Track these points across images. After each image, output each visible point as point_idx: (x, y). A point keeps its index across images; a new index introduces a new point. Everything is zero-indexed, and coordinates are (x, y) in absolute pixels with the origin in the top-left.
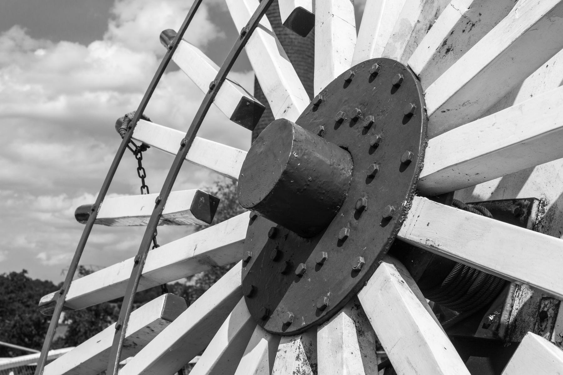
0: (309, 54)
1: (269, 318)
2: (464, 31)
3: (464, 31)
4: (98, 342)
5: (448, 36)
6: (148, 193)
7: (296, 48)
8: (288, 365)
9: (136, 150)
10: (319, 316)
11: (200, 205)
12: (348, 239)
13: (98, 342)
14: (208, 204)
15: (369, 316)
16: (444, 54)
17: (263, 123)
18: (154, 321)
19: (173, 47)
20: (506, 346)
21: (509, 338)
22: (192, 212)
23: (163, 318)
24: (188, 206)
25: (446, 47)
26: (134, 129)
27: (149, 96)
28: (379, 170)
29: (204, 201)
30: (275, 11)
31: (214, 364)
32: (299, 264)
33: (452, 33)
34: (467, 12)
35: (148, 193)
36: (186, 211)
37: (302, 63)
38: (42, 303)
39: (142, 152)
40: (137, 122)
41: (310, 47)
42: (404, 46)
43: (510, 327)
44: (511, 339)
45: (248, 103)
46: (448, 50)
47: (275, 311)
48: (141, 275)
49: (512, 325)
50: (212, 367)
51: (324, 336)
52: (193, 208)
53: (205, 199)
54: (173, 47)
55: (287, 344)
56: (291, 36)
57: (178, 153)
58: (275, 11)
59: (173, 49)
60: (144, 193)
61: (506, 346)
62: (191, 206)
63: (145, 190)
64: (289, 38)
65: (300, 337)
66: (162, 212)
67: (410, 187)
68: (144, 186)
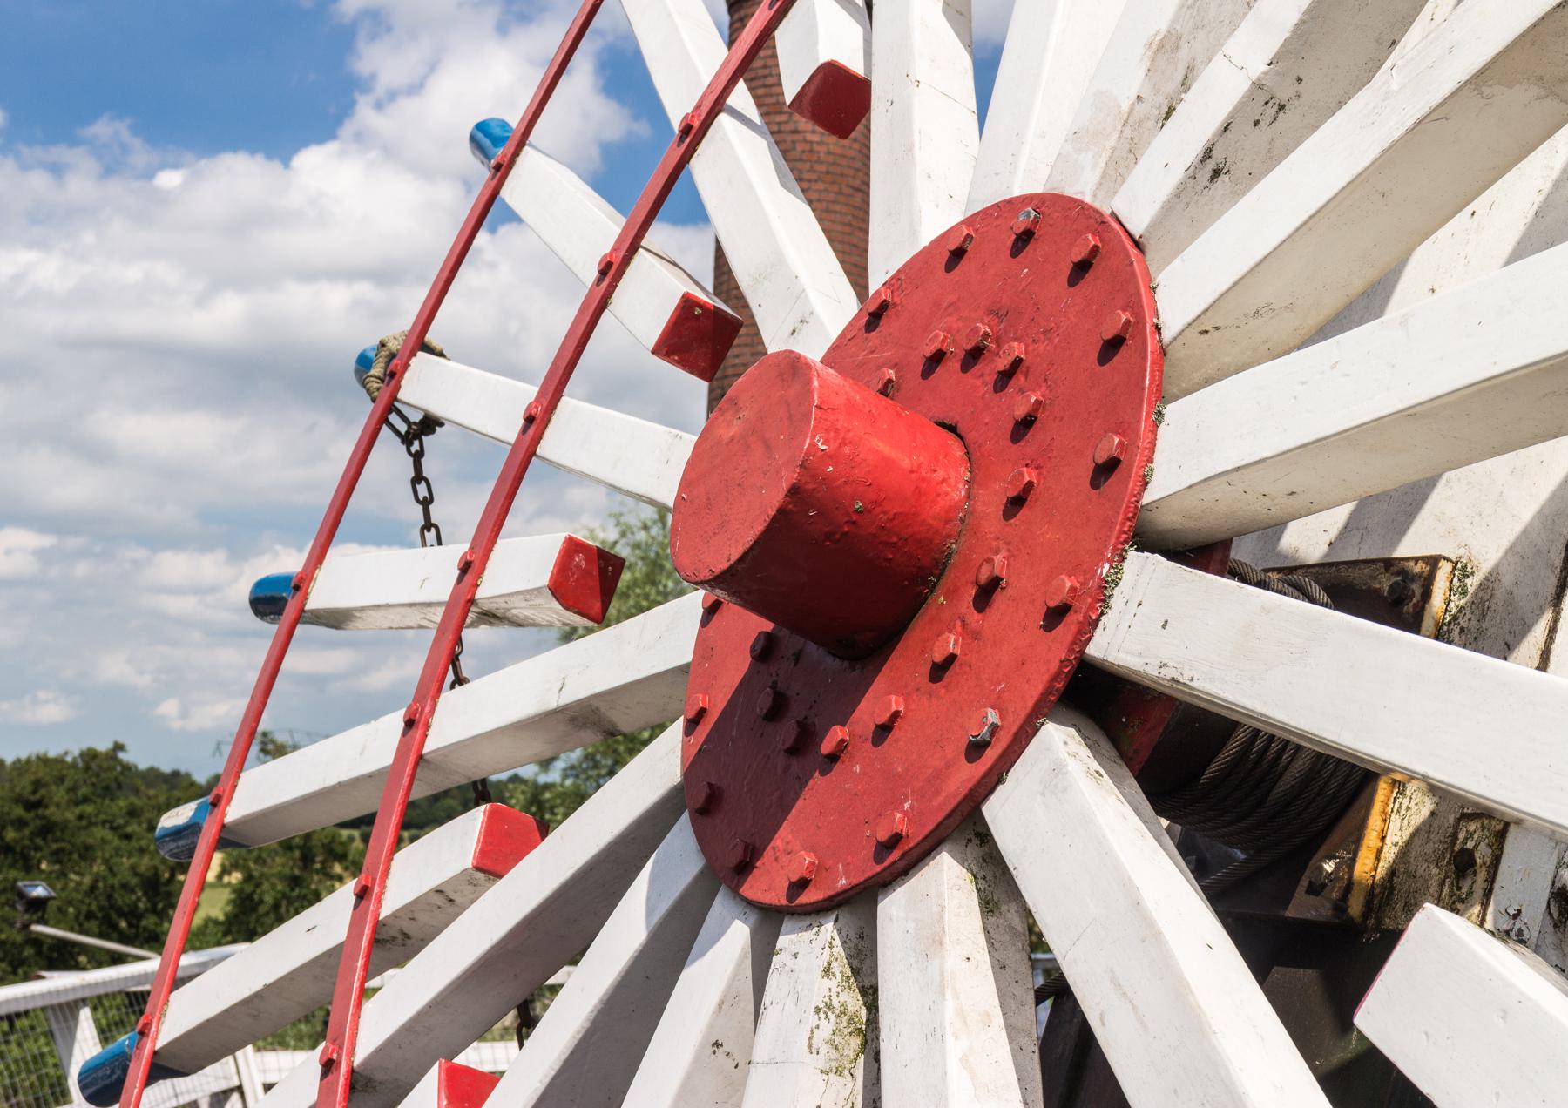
0: (857, 183)
2: (1256, 123)
3: (1256, 123)
5: (1215, 135)
6: (440, 543)
7: (823, 168)
11: (573, 574)
14: (596, 573)
17: (737, 361)
20: (1368, 940)
23: (477, 868)
25: (1210, 165)
26: (402, 377)
29: (583, 564)
30: (767, 72)
31: (611, 985)
33: (1226, 128)
34: (1265, 73)
35: (440, 543)
37: (837, 207)
38: (163, 828)
43: (1377, 891)
44: (1379, 921)
45: (698, 311)
46: (1216, 173)
50: (604, 994)
53: (587, 560)
55: (800, 934)
56: (810, 137)
58: (767, 72)
61: (1368, 940)
62: (551, 577)
63: (431, 536)
65: (834, 916)
66: (474, 594)
68: (428, 525)
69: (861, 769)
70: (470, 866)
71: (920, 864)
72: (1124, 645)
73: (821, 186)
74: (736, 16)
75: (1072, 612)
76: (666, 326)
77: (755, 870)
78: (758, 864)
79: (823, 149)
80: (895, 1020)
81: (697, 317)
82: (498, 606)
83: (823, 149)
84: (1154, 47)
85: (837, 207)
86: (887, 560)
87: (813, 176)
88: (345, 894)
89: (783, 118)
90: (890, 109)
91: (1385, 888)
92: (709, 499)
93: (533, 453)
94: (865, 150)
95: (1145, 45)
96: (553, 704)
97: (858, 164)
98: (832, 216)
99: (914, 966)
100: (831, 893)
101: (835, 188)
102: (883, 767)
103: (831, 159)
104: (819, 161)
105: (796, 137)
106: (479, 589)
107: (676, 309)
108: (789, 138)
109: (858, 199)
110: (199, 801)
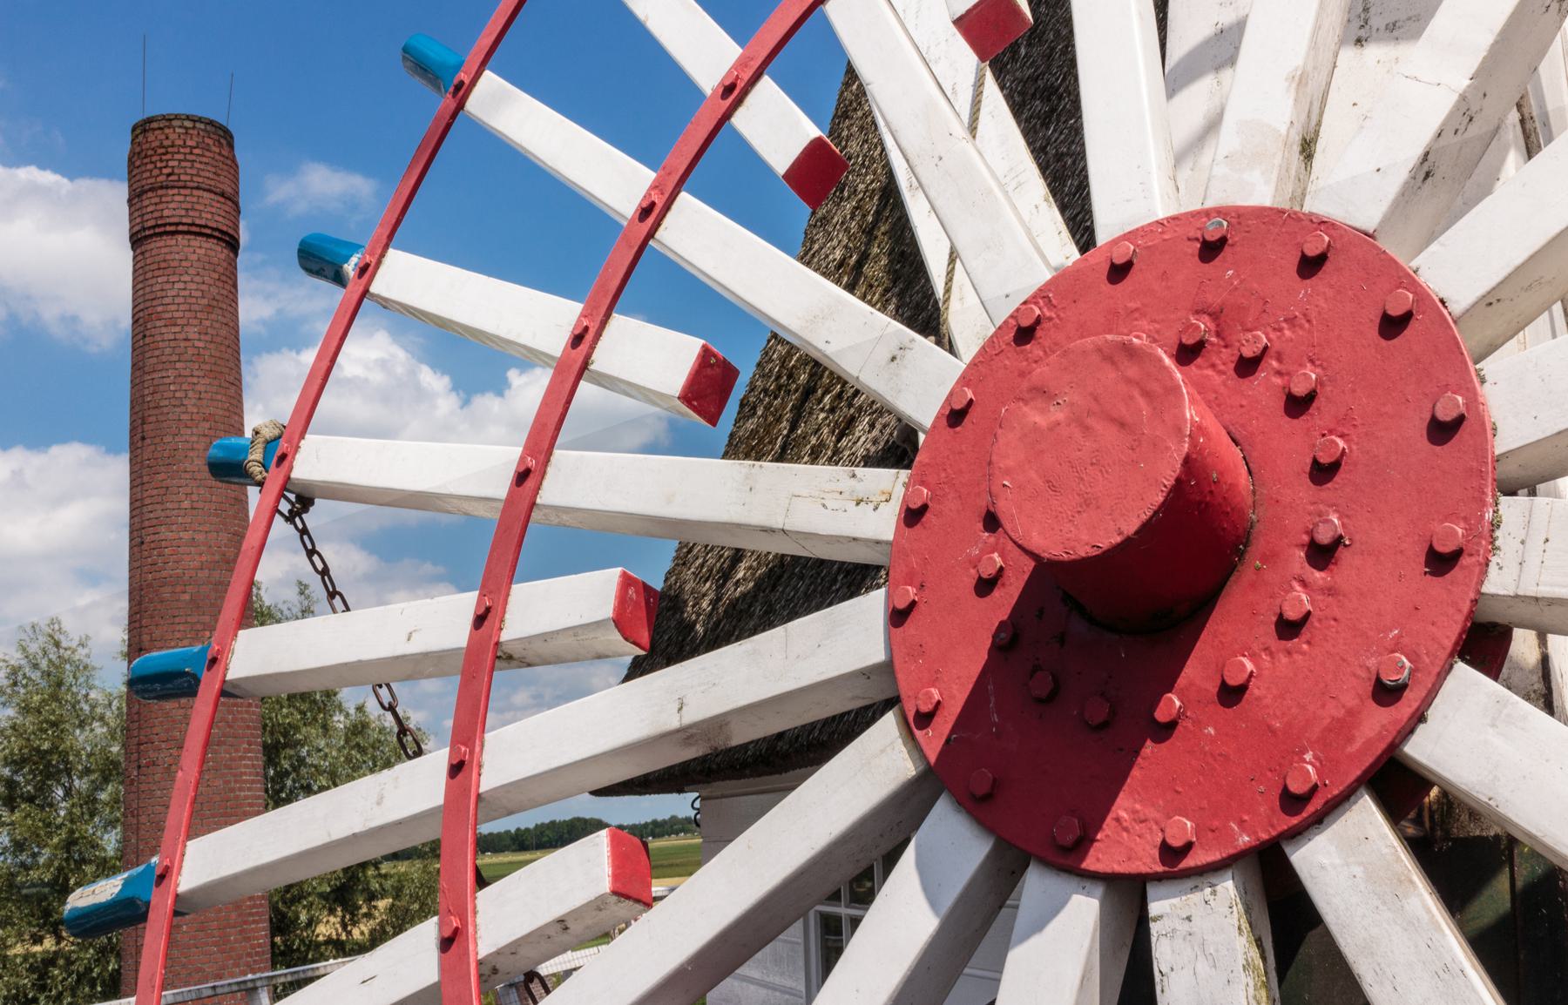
0: (231, 379)
1: (1093, 840)
4: (364, 982)
6: (348, 609)
7: (208, 367)
8: (1217, 951)
9: (290, 511)
10: (1301, 813)
12: (1312, 619)
13: (364, 982)
14: (643, 604)
15: (1484, 795)
16: (1419, 184)
17: (152, 515)
18: (585, 901)
19: (373, 264)
20: (1440, 849)
21: (1441, 829)
22: (617, 626)
23: (615, 893)
24: (607, 610)
25: (1425, 168)
26: (294, 458)
27: (604, 316)
28: (1351, 451)
29: (634, 596)
30: (164, 294)
32: (1162, 696)
33: (1440, 134)
34: (1469, 86)
35: (348, 609)
36: (598, 624)
37: (219, 397)
38: (74, 909)
39: (304, 516)
40: (299, 442)
41: (231, 365)
42: (1274, 176)
43: (1435, 807)
44: (1447, 832)
45: (713, 361)
46: (1427, 175)
47: (1109, 820)
48: (479, 796)
49: (1438, 801)
50: (894, 992)
51: (1325, 861)
52: (617, 615)
53: (636, 592)
54: (373, 264)
56: (197, 344)
57: (511, 493)
58: (164, 294)
59: (371, 269)
60: (338, 610)
61: (1440, 849)
63: (337, 601)
64: (194, 346)
67: (1490, 475)
68: (332, 594)
69: (1215, 729)
70: (608, 891)
71: (1337, 812)
72: (1541, 578)
73: (207, 381)
74: (138, 251)
75: (1465, 555)
76: (690, 374)
77: (1096, 844)
78: (1099, 837)
79: (208, 353)
80: (1379, 965)
81: (712, 366)
82: (516, 651)
83: (208, 353)
84: (1297, 79)
85: (219, 397)
86: (1224, 529)
87: (201, 373)
88: (425, 934)
89: (177, 329)
90: (940, 163)
91: (1443, 803)
92: (1048, 482)
93: (533, 504)
94: (236, 354)
95: (1286, 79)
96: (673, 722)
97: (231, 365)
98: (215, 404)
99: (1381, 907)
100: (1232, 851)
101: (216, 382)
102: (1249, 724)
103: (213, 360)
104: (204, 362)
105: (187, 344)
106: (503, 632)
107: (698, 358)
108: (183, 344)
109: (233, 390)
110: (126, 875)
